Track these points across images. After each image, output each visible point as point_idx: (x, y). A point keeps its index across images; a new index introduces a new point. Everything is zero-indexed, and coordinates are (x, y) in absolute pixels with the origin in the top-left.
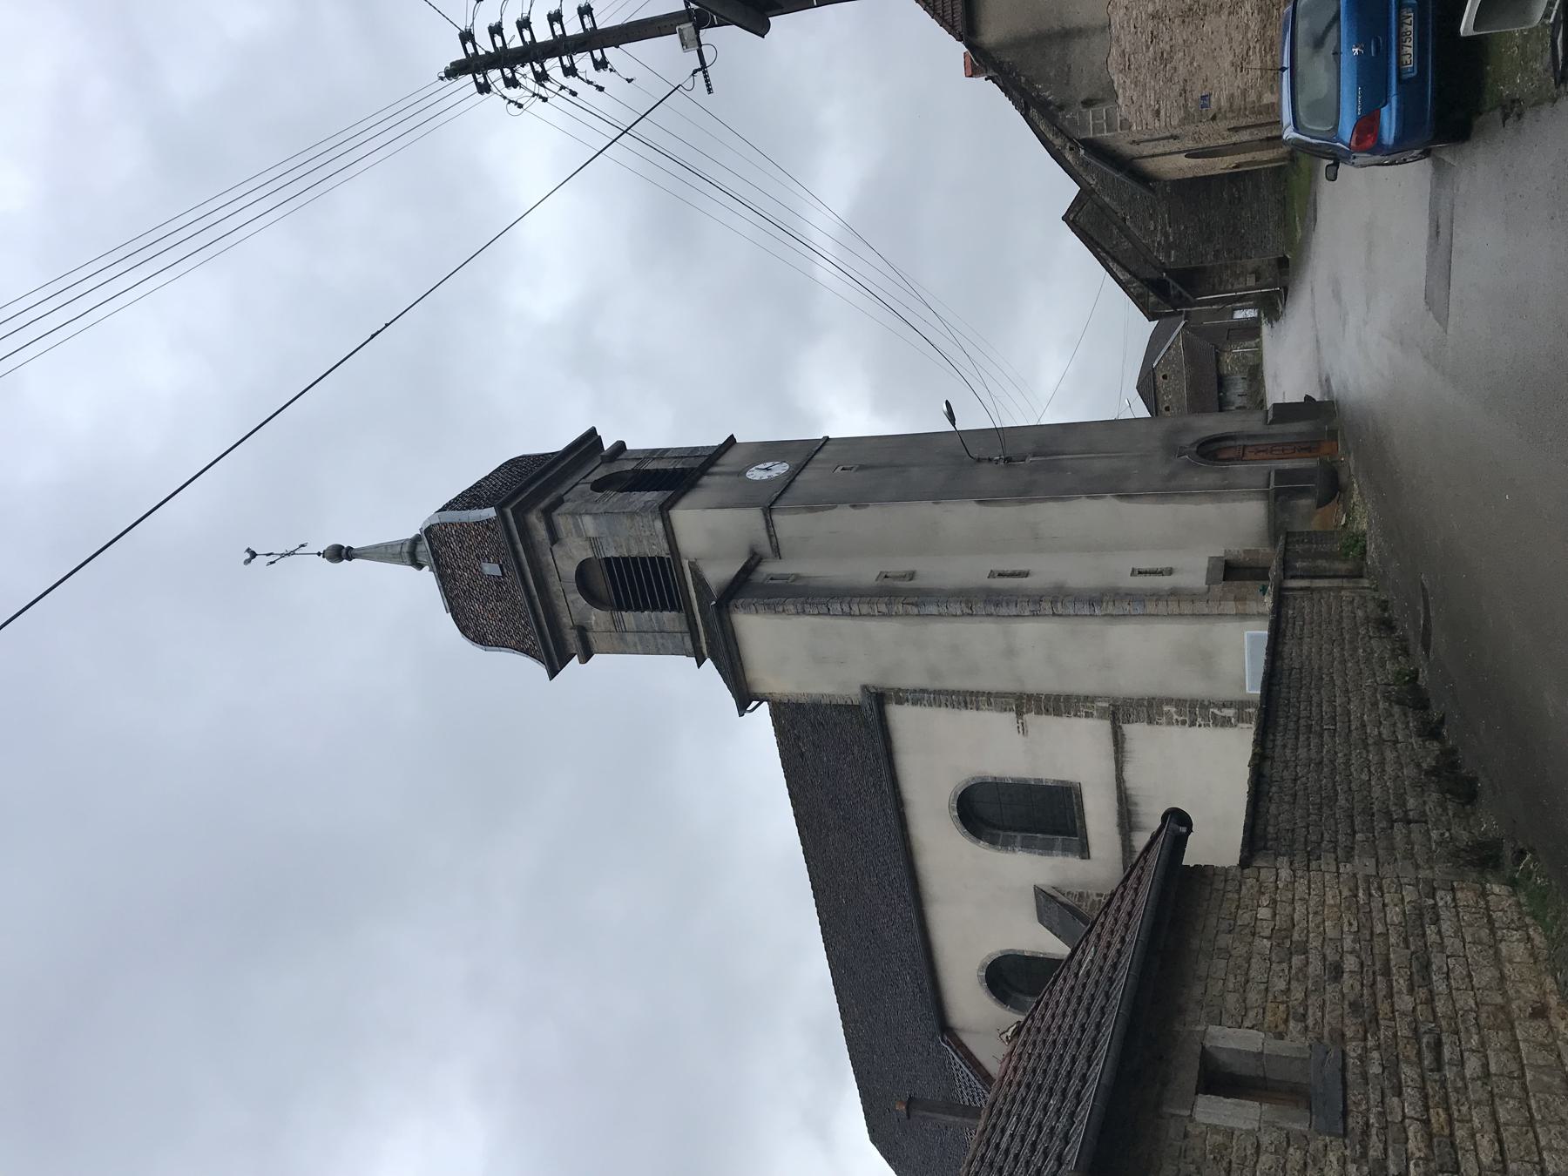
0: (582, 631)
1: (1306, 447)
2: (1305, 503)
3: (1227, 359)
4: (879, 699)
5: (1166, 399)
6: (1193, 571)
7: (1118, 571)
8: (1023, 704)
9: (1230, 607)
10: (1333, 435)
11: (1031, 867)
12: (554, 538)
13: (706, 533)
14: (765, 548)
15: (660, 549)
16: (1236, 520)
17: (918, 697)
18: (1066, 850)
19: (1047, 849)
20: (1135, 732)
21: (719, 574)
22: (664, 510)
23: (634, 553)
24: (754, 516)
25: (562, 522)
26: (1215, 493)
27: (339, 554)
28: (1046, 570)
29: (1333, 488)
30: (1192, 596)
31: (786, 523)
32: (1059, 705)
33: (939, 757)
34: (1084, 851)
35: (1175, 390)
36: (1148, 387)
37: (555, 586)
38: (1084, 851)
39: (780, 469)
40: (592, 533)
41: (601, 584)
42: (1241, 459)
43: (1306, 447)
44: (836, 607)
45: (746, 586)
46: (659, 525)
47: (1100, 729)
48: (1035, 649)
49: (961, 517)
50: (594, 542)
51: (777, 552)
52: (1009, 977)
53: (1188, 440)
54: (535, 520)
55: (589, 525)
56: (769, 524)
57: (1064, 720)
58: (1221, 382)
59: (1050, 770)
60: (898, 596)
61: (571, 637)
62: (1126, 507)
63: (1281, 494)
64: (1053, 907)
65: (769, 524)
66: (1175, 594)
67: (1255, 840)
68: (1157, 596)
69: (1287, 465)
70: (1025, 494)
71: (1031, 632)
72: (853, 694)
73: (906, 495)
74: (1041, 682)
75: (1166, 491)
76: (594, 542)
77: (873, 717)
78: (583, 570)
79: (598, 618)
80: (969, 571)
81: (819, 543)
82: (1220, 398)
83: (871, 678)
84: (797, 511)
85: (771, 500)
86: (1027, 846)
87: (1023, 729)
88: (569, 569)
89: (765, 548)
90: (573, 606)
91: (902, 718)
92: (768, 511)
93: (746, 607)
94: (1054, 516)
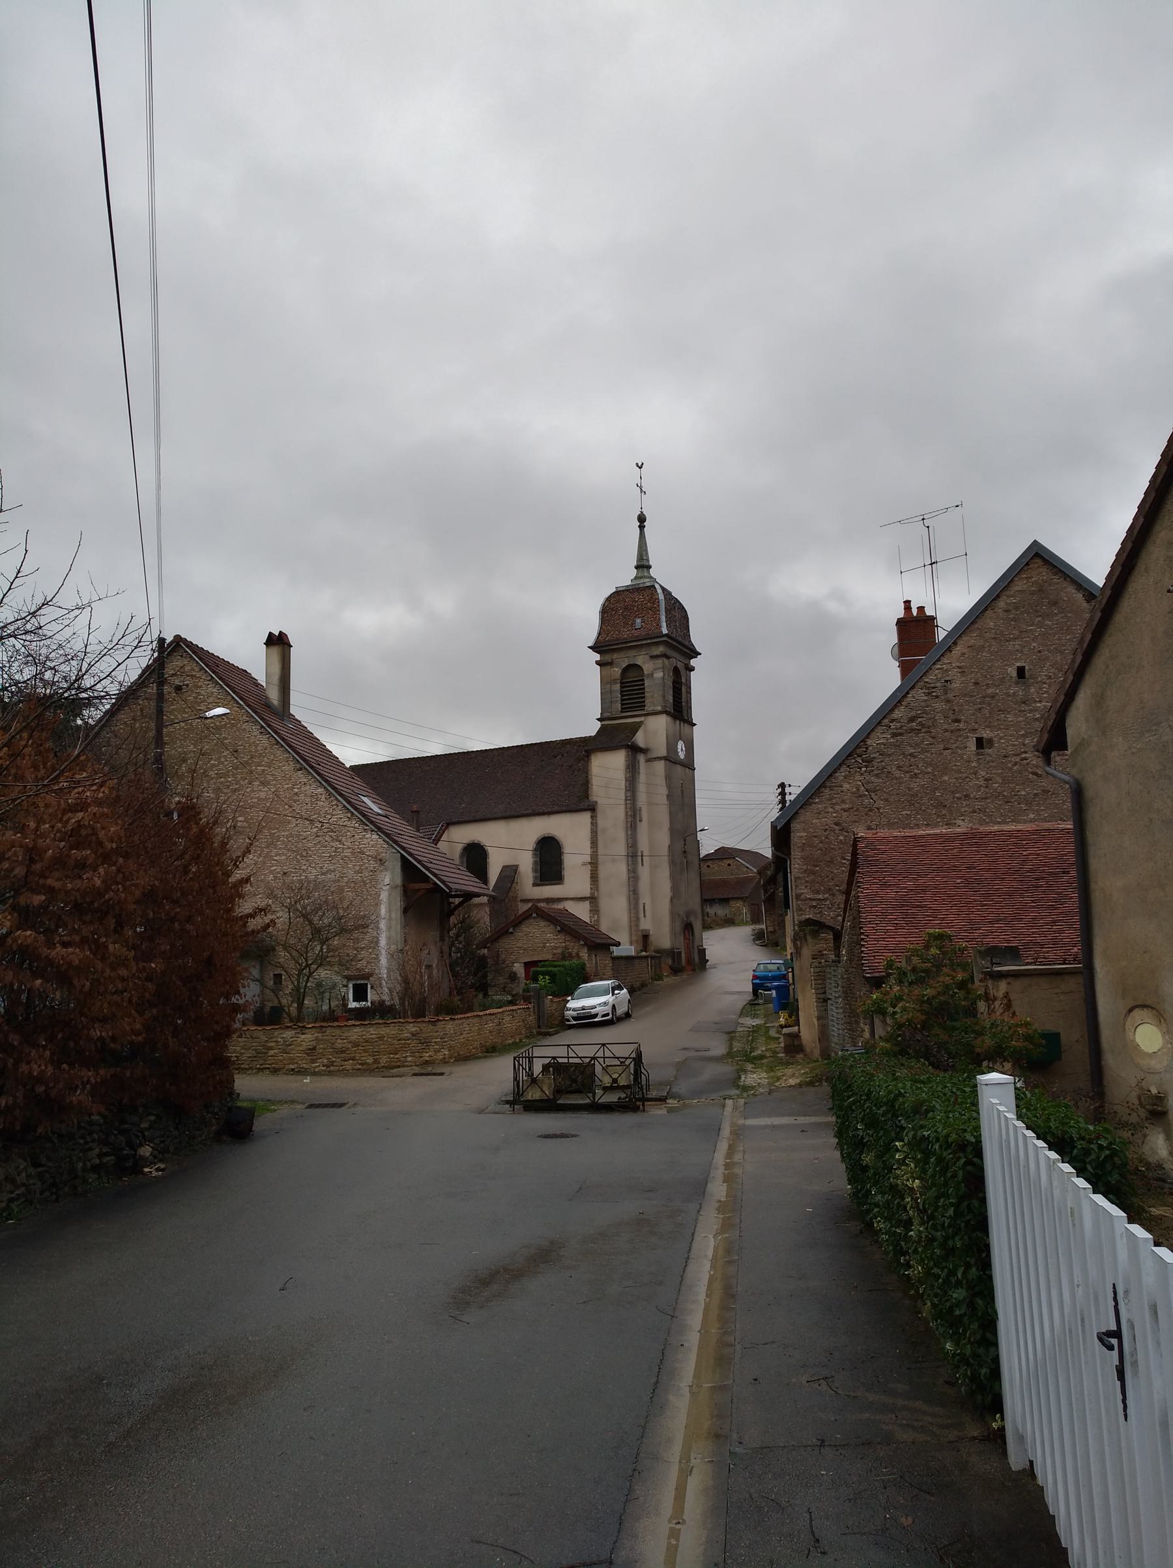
0: (611, 664)
1: (690, 961)
2: (670, 962)
3: (739, 904)
4: (592, 809)
5: (715, 866)
6: (646, 924)
7: (645, 898)
8: (594, 865)
9: (634, 938)
10: (694, 970)
11: (526, 863)
12: (652, 657)
13: (655, 729)
14: (650, 756)
15: (649, 708)
16: (664, 938)
17: (594, 824)
18: (535, 878)
19: (535, 870)
20: (587, 904)
21: (640, 739)
22: (667, 713)
23: (647, 694)
24: (663, 752)
25: (659, 662)
26: (673, 932)
27: (642, 519)
28: (644, 872)
29: (676, 970)
30: (637, 925)
31: (660, 766)
32: (594, 878)
33: (572, 831)
34: (535, 885)
35: (718, 872)
36: (724, 854)
37: (632, 653)
38: (535, 885)
39: (682, 755)
40: (655, 675)
41: (632, 676)
42: (685, 938)
43: (690, 961)
44: (629, 794)
45: (635, 750)
46: (659, 708)
47: (586, 892)
48: (615, 871)
49: (663, 838)
50: (651, 675)
51: (648, 760)
52: (475, 856)
53: (692, 919)
54: (661, 649)
55: (659, 675)
56: (660, 758)
57: (589, 880)
58: (725, 901)
59: (567, 873)
60: (633, 816)
61: (608, 658)
62: (668, 899)
63: (673, 954)
64: (510, 873)
65: (660, 758)
66: (638, 919)
67: (615, 959)
68: (637, 913)
69: (683, 955)
70: (672, 863)
71: (622, 868)
72: (593, 798)
73: (672, 815)
74: (603, 872)
75: (673, 914)
76: (651, 675)
77: (582, 806)
78: (639, 668)
79: (617, 671)
80: (643, 845)
81: (653, 776)
82: (714, 900)
83: (599, 808)
84: (666, 770)
85: (670, 759)
86: (535, 863)
87: (584, 864)
88: (639, 661)
89: (650, 756)
90: (623, 660)
91: (586, 817)
92: (665, 759)
93: (628, 756)
94: (664, 873)
